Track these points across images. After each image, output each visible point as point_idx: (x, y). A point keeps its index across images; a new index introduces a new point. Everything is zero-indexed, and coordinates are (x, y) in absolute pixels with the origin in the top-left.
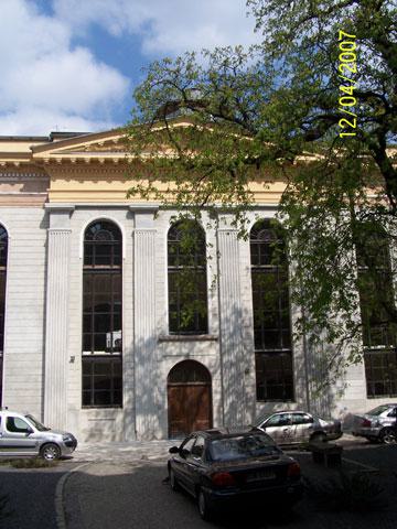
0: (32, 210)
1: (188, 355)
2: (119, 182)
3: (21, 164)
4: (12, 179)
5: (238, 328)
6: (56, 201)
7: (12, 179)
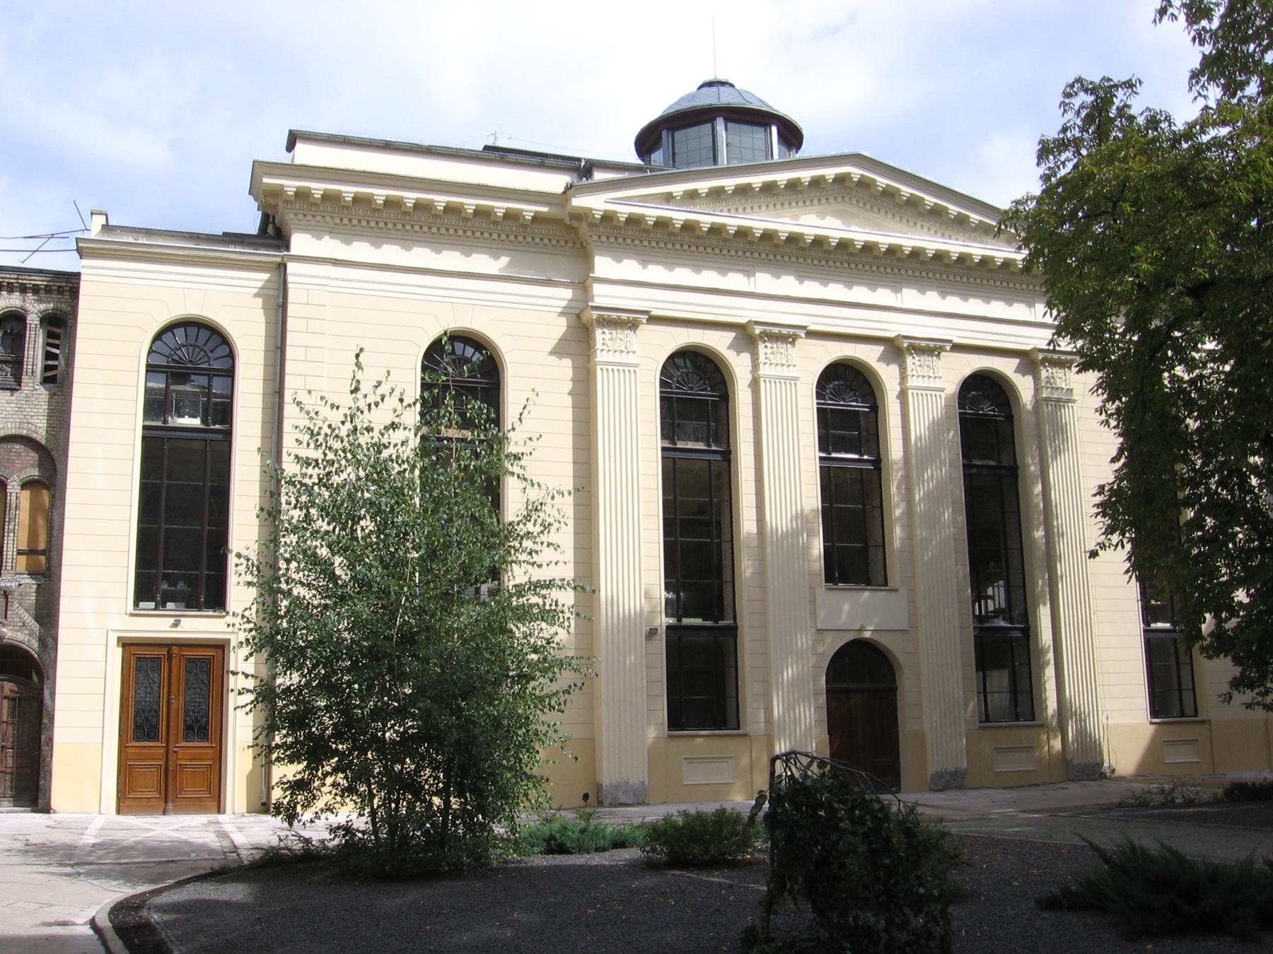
3: (537, 218)
6: (603, 296)
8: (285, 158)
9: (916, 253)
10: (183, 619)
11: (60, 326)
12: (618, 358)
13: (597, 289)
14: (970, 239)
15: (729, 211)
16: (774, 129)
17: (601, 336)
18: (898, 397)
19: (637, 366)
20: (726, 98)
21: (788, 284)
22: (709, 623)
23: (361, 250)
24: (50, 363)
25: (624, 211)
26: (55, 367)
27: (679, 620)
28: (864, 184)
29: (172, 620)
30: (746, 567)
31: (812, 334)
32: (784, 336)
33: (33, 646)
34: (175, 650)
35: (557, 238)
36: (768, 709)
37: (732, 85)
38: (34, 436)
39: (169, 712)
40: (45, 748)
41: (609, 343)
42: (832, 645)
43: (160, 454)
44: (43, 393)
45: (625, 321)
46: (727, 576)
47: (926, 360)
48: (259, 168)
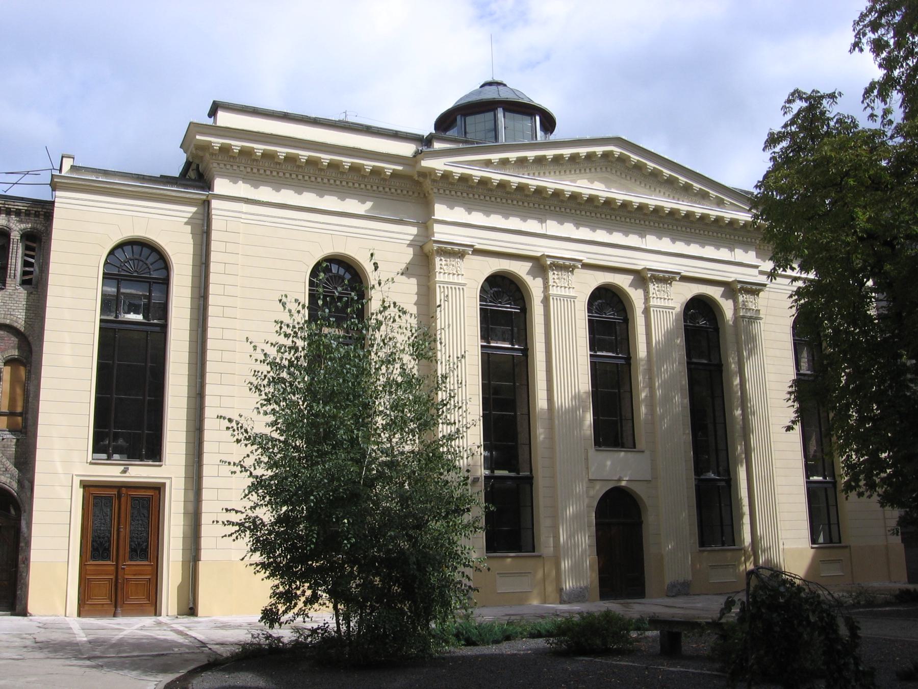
2: (604, 232)
3: (395, 174)
6: (441, 233)
8: (210, 121)
9: (658, 210)
10: (130, 467)
11: (38, 242)
12: (451, 279)
13: (437, 228)
14: (691, 201)
15: (529, 174)
16: (538, 118)
18: (643, 313)
19: (464, 285)
20: (504, 95)
21: (568, 229)
22: (513, 474)
23: (265, 193)
24: (27, 269)
25: (458, 171)
26: (31, 273)
27: (492, 472)
28: (622, 159)
29: (122, 468)
30: (540, 433)
31: (586, 266)
32: (566, 266)
33: (13, 486)
34: (124, 490)
35: (405, 189)
36: (556, 537)
37: (505, 85)
38: (15, 325)
39: (122, 538)
40: (21, 566)
41: (445, 267)
42: (600, 490)
43: (111, 339)
44: (22, 293)
45: (456, 252)
46: (522, 438)
47: (662, 286)
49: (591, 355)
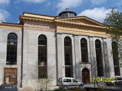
0: (21, 28)
1: (85, 67)
2: (84, 30)
3: (51, 22)
4: (31, 23)
5: (94, 61)
6: (58, 31)
7: (31, 23)
8: (23, 15)
17: (58, 35)
28: (85, 19)
35: (53, 25)
48: (20, 16)
49: (64, 47)
